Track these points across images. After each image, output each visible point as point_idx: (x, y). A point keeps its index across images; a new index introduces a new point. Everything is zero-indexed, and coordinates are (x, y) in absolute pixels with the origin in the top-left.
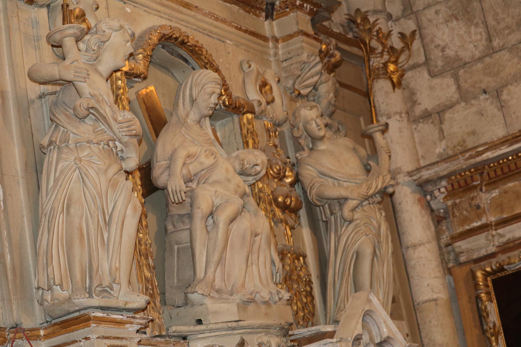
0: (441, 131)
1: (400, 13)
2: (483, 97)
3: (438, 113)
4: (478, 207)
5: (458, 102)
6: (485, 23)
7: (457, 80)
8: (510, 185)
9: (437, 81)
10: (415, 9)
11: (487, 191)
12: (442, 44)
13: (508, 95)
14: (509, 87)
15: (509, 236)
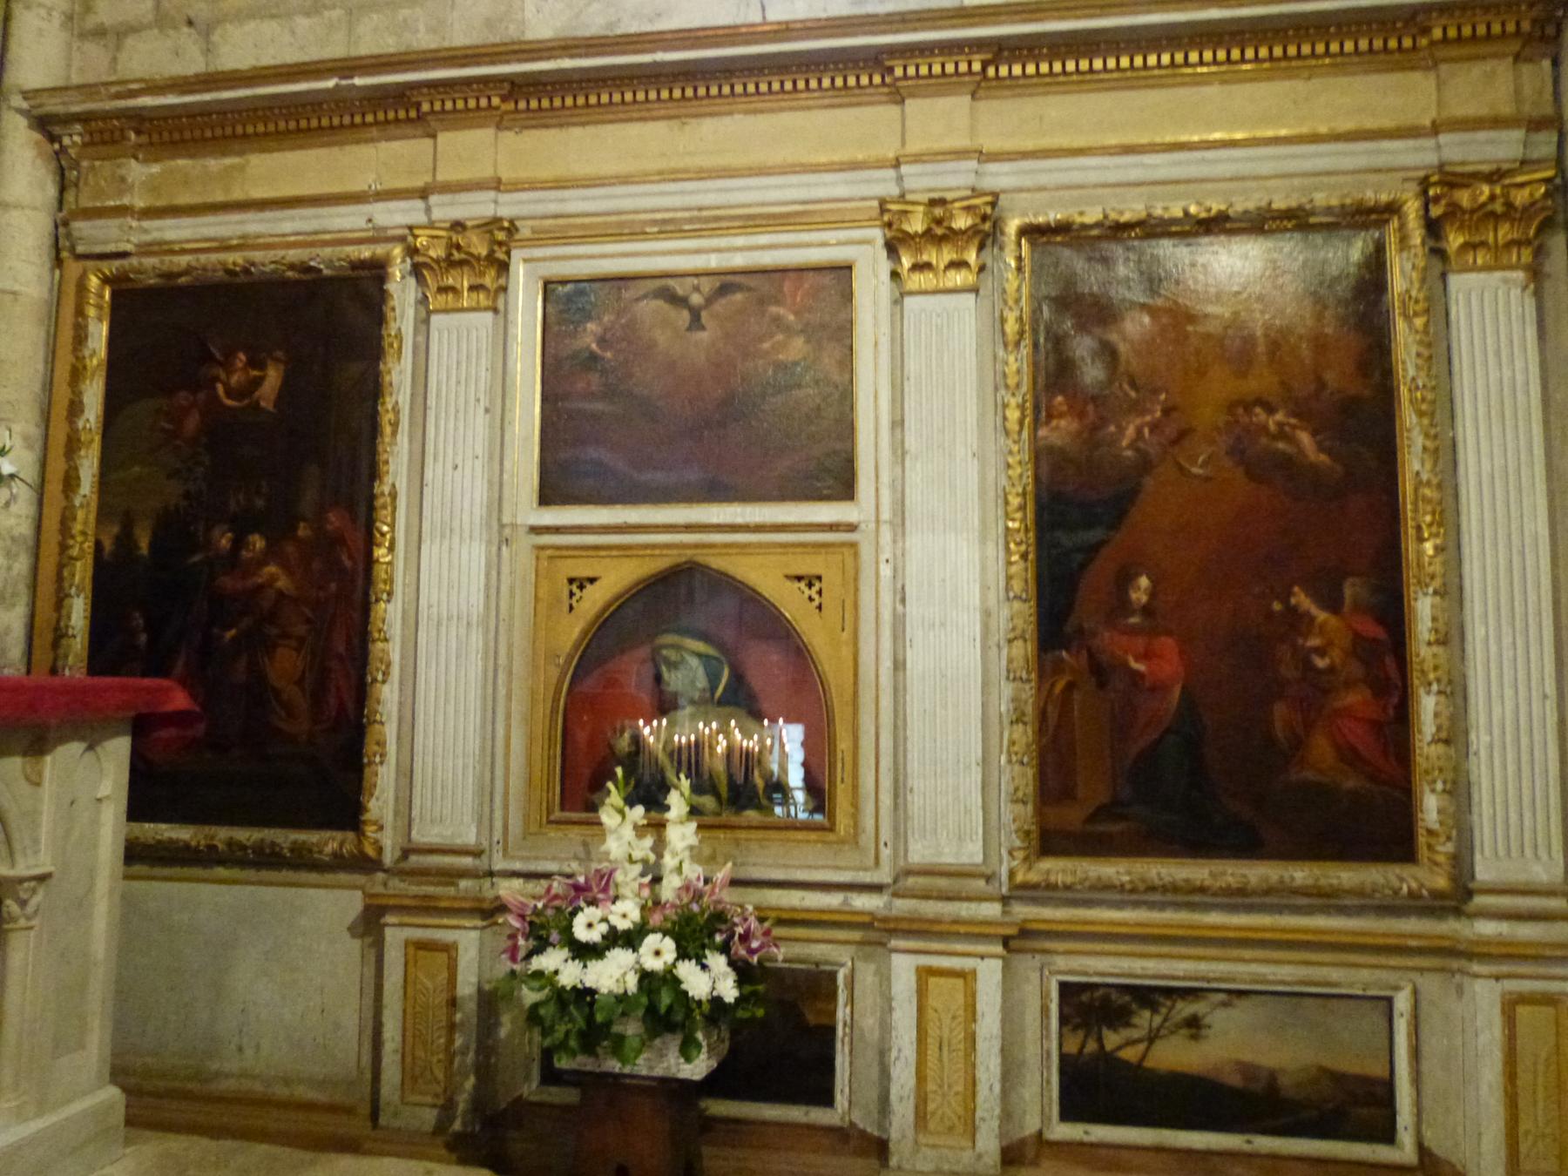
0: (114, 60)
2: (185, 30)
3: (118, 34)
5: (149, 27)
8: (181, 162)
11: (146, 161)
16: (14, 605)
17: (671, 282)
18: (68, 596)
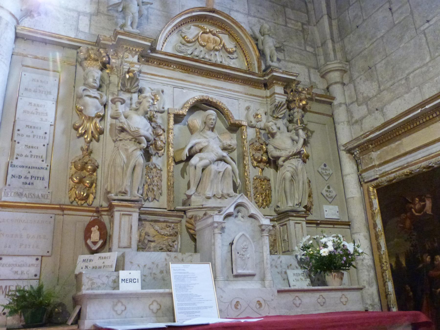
0: (362, 128)
1: (348, 82)
2: (376, 112)
4: (371, 158)
6: (378, 80)
7: (367, 106)
8: (384, 148)
9: (360, 107)
10: (353, 79)
12: (362, 91)
13: (386, 109)
14: (386, 106)
15: (383, 171)
16: (372, 286)
17: (332, 199)
18: (386, 282)
